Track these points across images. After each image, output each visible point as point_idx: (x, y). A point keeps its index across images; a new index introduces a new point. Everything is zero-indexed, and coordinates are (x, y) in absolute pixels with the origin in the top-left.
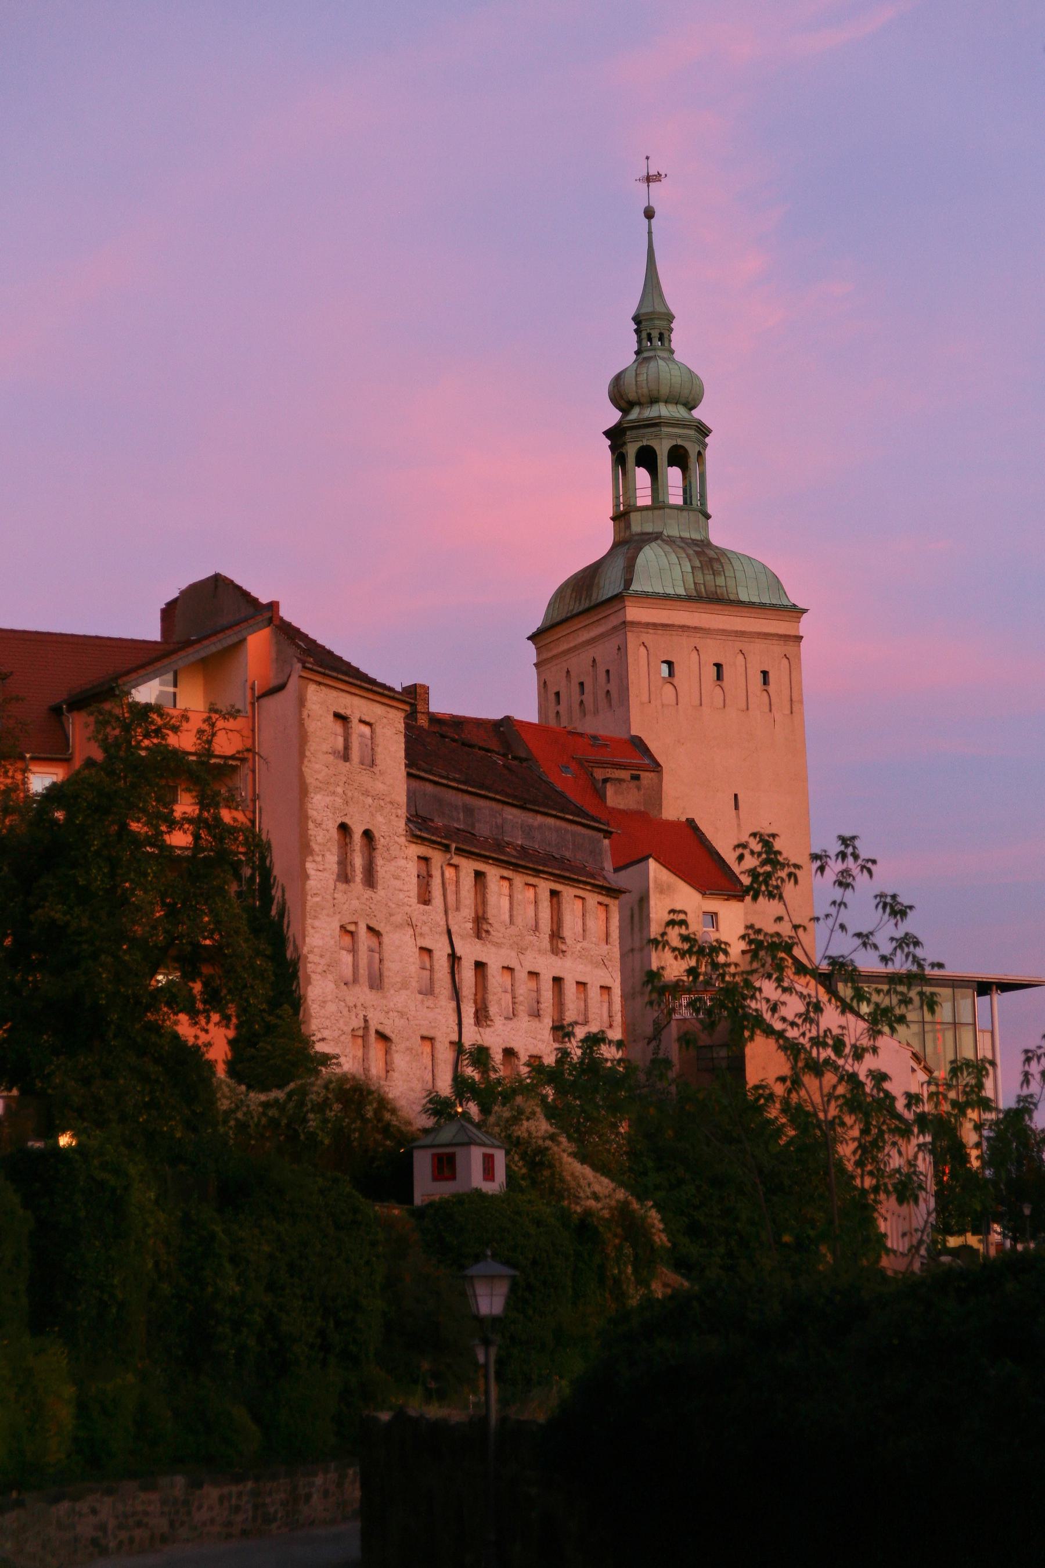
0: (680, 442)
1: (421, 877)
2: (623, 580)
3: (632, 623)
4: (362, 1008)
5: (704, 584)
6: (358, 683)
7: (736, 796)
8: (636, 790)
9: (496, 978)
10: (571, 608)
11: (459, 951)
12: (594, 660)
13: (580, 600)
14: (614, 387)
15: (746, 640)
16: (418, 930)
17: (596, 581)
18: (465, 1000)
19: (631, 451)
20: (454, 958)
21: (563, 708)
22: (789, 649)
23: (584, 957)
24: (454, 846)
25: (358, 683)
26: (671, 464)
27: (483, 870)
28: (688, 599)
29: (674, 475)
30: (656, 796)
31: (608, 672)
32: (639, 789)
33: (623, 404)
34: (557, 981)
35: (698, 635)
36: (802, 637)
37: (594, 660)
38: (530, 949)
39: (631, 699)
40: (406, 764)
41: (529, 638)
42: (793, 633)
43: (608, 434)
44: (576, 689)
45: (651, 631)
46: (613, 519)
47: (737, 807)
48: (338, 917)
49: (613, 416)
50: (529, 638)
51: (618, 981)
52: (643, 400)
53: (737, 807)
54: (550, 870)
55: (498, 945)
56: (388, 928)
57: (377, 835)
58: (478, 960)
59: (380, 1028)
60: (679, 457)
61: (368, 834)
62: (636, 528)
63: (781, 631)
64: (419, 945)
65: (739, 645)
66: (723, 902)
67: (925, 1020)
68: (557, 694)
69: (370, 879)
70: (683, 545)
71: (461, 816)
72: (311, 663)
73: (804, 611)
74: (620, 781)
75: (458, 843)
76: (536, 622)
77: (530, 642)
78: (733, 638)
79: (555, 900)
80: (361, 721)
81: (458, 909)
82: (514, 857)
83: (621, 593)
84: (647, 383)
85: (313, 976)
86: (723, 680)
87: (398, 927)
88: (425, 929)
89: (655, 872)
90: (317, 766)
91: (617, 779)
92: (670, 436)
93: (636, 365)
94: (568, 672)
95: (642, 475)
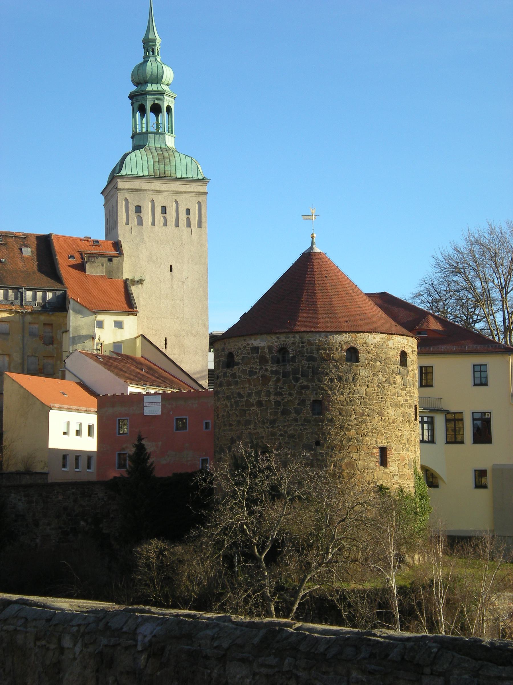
0: (156, 102)
3: (120, 189)
7: (171, 266)
8: (101, 266)
15: (179, 195)
22: (201, 199)
23: (455, 305)
28: (149, 177)
45: (130, 192)
47: (171, 271)
49: (134, 88)
52: (142, 82)
53: (171, 271)
65: (175, 197)
67: (482, 370)
73: (208, 181)
78: (172, 194)
89: (73, 304)
92: (151, 99)
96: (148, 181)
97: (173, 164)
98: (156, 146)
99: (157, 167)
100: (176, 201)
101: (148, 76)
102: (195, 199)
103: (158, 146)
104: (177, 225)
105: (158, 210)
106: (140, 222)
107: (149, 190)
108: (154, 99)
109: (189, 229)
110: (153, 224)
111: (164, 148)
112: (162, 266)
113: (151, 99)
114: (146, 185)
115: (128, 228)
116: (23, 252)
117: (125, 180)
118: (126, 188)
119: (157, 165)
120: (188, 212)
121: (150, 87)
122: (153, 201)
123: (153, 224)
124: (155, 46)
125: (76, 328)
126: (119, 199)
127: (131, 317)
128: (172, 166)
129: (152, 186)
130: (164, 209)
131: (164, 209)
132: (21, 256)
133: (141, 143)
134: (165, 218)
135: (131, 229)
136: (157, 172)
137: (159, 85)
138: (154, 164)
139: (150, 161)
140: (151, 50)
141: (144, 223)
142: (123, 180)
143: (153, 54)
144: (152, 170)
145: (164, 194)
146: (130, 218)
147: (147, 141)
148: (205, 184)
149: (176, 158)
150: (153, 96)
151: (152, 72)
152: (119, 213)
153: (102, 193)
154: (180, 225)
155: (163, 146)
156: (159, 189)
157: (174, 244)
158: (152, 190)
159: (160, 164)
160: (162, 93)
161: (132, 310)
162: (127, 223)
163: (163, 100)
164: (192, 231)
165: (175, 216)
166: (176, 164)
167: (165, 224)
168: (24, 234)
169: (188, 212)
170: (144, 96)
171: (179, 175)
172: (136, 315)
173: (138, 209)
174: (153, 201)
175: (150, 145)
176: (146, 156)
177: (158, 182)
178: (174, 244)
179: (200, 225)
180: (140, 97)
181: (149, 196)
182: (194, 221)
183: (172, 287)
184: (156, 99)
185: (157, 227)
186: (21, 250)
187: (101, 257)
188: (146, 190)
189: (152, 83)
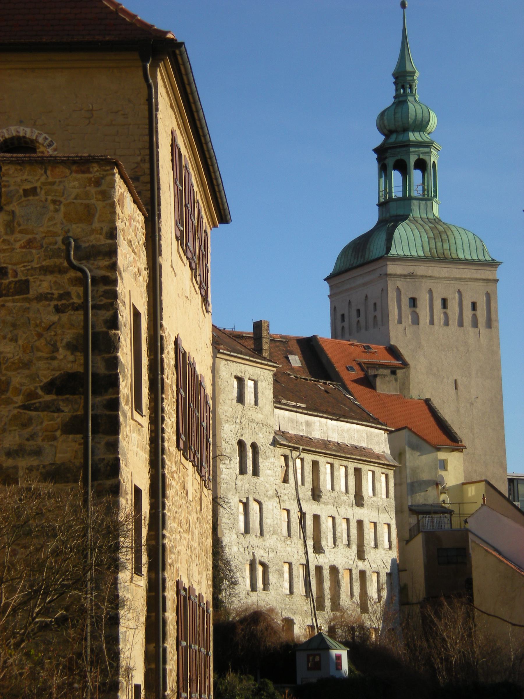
0: (422, 157)
1: (283, 467)
2: (385, 247)
3: (391, 275)
4: (252, 548)
5: (436, 248)
6: (248, 358)
7: (456, 381)
8: (394, 381)
9: (326, 525)
10: (352, 262)
11: (304, 509)
12: (366, 296)
13: (358, 258)
14: (380, 120)
16: (281, 499)
17: (368, 246)
18: (308, 538)
19: (390, 162)
20: (303, 515)
21: (346, 324)
22: (490, 288)
24: (301, 447)
25: (248, 358)
26: (415, 168)
27: (317, 460)
29: (416, 175)
30: (405, 386)
31: (375, 304)
32: (396, 380)
33: (386, 132)
34: (360, 523)
35: (432, 281)
36: (498, 280)
37: (366, 296)
38: (343, 505)
39: (390, 321)
40: (274, 401)
41: (325, 280)
42: (491, 277)
43: (376, 150)
44: (354, 313)
45: (403, 279)
46: (378, 205)
48: (238, 495)
49: (379, 139)
50: (325, 280)
51: (394, 519)
54: (354, 457)
55: (326, 504)
56: (266, 499)
57: (259, 445)
58: (315, 513)
59: (262, 560)
60: (421, 165)
61: (254, 446)
62: (393, 212)
63: (483, 277)
64: (282, 507)
66: (449, 453)
68: (343, 316)
69: (256, 473)
70: (422, 223)
71: (304, 428)
72: (223, 349)
73: (499, 263)
74: (385, 376)
75: (303, 446)
76: (329, 269)
77: (326, 282)
79: (357, 473)
80: (249, 379)
81: (303, 484)
82: (335, 451)
83: (383, 256)
84: (402, 119)
85: (225, 531)
86: (447, 308)
87: (270, 498)
88: (286, 498)
90: (226, 408)
91: (382, 375)
92: (415, 152)
93: (394, 107)
94: (350, 302)
95: (396, 176)
96: (425, 265)
97: (452, 241)
98: (422, 216)
99: (433, 245)
100: (459, 292)
101: (411, 121)
102: (482, 287)
103: (424, 216)
104: (461, 324)
105: (438, 304)
106: (416, 321)
107: (426, 276)
108: (418, 153)
109: (476, 330)
110: (432, 322)
111: (432, 219)
112: (445, 380)
113: (415, 152)
114: (421, 269)
115: (400, 327)
116: (291, 362)
117: (397, 263)
118: (398, 273)
119: (432, 242)
120: (474, 306)
121: (413, 136)
122: (430, 291)
123: (432, 322)
124: (414, 80)
125: (414, 471)
126: (389, 289)
127: (456, 454)
128: (451, 244)
129: (430, 272)
130: (444, 302)
131: (444, 302)
132: (290, 368)
133: (401, 212)
134: (446, 314)
135: (405, 329)
136: (434, 252)
137: (422, 133)
138: (429, 241)
139: (424, 237)
140: (408, 86)
141: (421, 322)
142: (394, 263)
143: (411, 92)
144: (427, 249)
145: (444, 282)
146: (403, 315)
147: (410, 210)
148: (494, 269)
149: (454, 232)
150: (417, 149)
151: (416, 116)
152: (390, 308)
153: (327, 279)
154: (465, 324)
155: (431, 216)
156: (438, 276)
157: (458, 350)
158: (430, 277)
159: (436, 240)
160: (428, 145)
161: (457, 444)
162: (400, 322)
163: (429, 154)
164: (480, 333)
165: (458, 311)
166: (457, 242)
167: (447, 323)
168: (282, 337)
169: (474, 306)
170: (404, 149)
171: (461, 256)
172: (462, 452)
173: (413, 302)
174: (430, 291)
175: (415, 215)
176: (417, 231)
177: (437, 265)
178: (458, 350)
179: (489, 324)
180: (398, 150)
181: (427, 284)
182: (482, 319)
183: (458, 411)
184: (422, 153)
185: (436, 327)
186: (287, 358)
187: (382, 368)
188: (422, 276)
189: (413, 131)
